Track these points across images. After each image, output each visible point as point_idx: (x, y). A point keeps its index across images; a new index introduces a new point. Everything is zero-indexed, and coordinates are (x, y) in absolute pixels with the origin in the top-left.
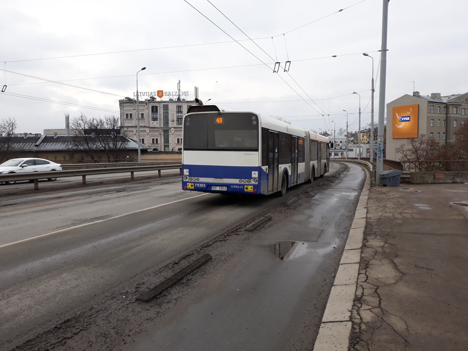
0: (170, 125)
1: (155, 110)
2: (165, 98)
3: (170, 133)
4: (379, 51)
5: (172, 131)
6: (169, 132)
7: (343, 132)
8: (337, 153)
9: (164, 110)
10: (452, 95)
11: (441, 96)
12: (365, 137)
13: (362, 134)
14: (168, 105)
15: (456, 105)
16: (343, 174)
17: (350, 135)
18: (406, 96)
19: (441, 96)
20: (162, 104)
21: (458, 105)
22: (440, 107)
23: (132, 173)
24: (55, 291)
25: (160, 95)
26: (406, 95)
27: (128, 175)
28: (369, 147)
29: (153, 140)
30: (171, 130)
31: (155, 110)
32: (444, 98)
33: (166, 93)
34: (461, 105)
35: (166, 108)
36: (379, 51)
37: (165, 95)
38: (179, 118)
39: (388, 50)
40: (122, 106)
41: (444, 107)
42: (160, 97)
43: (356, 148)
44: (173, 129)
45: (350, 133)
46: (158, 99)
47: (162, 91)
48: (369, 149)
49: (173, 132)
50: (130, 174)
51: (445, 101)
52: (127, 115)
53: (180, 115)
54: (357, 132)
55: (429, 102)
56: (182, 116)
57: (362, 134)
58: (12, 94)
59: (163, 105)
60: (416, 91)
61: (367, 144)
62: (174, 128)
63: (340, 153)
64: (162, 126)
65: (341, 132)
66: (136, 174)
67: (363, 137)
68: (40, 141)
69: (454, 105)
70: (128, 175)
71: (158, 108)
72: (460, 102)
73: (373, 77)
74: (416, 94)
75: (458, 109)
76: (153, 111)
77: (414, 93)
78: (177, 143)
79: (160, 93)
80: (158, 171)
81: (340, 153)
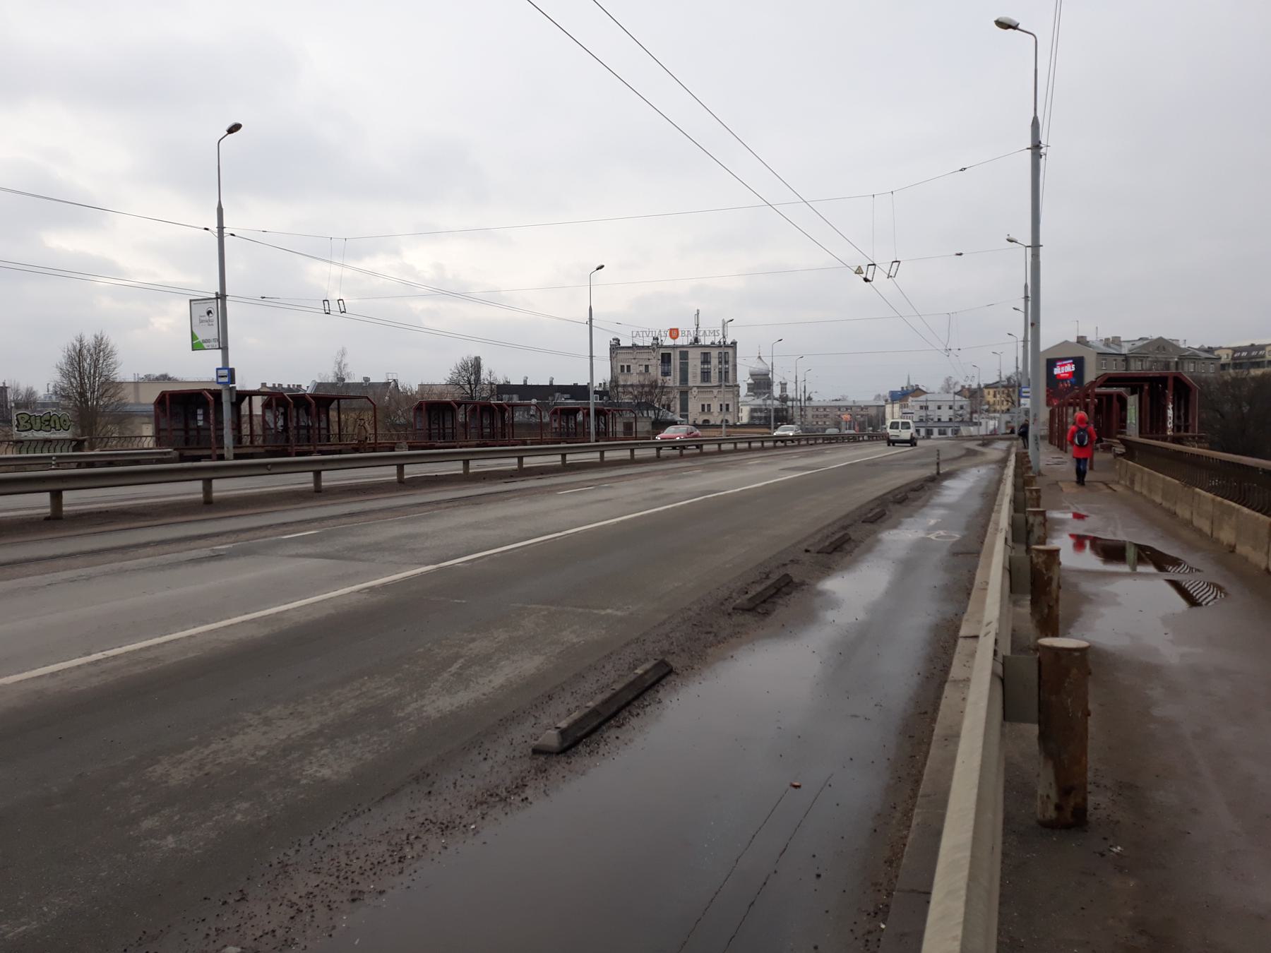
0: (690, 384)
1: (666, 359)
2: (682, 341)
3: (690, 396)
4: (1028, 149)
5: (693, 393)
6: (689, 393)
7: (952, 386)
8: (945, 430)
9: (681, 359)
10: (1141, 339)
11: (1122, 339)
12: (998, 396)
13: (992, 391)
14: (687, 352)
15: (1141, 357)
16: (242, 948)
17: (967, 392)
18: (1066, 343)
19: (1122, 339)
20: (678, 350)
21: (1144, 357)
22: (1115, 360)
23: (56, 496)
24: (1016, 430)
25: (674, 335)
26: (1066, 341)
27: (39, 503)
28: (1009, 419)
29: (703, 406)
30: (693, 391)
31: (666, 359)
32: (1126, 344)
33: (683, 332)
34: (1147, 357)
35: (684, 356)
36: (1028, 149)
37: (682, 336)
38: (704, 372)
39: (1042, 246)
40: (615, 353)
41: (1123, 360)
42: (674, 338)
43: (988, 420)
44: (695, 389)
45: (967, 387)
46: (668, 342)
47: (677, 330)
48: (1009, 422)
49: (695, 394)
50: (45, 498)
51: (1125, 351)
52: (622, 367)
53: (706, 366)
54: (982, 386)
55: (1098, 353)
56: (710, 369)
57: (992, 391)
58: (393, 324)
59: (680, 352)
60: (1080, 335)
61: (1006, 413)
62: (698, 387)
63: (950, 429)
64: (678, 384)
65: (949, 385)
66: (73, 500)
67: (995, 396)
68: (1122, 436)
69: (1137, 357)
70: (39, 503)
71: (672, 357)
72: (1146, 352)
73: (1038, 115)
74: (1080, 340)
75: (1144, 363)
76: (663, 361)
77: (1078, 337)
78: (700, 410)
79: (674, 333)
80: (311, 474)
81: (950, 429)
